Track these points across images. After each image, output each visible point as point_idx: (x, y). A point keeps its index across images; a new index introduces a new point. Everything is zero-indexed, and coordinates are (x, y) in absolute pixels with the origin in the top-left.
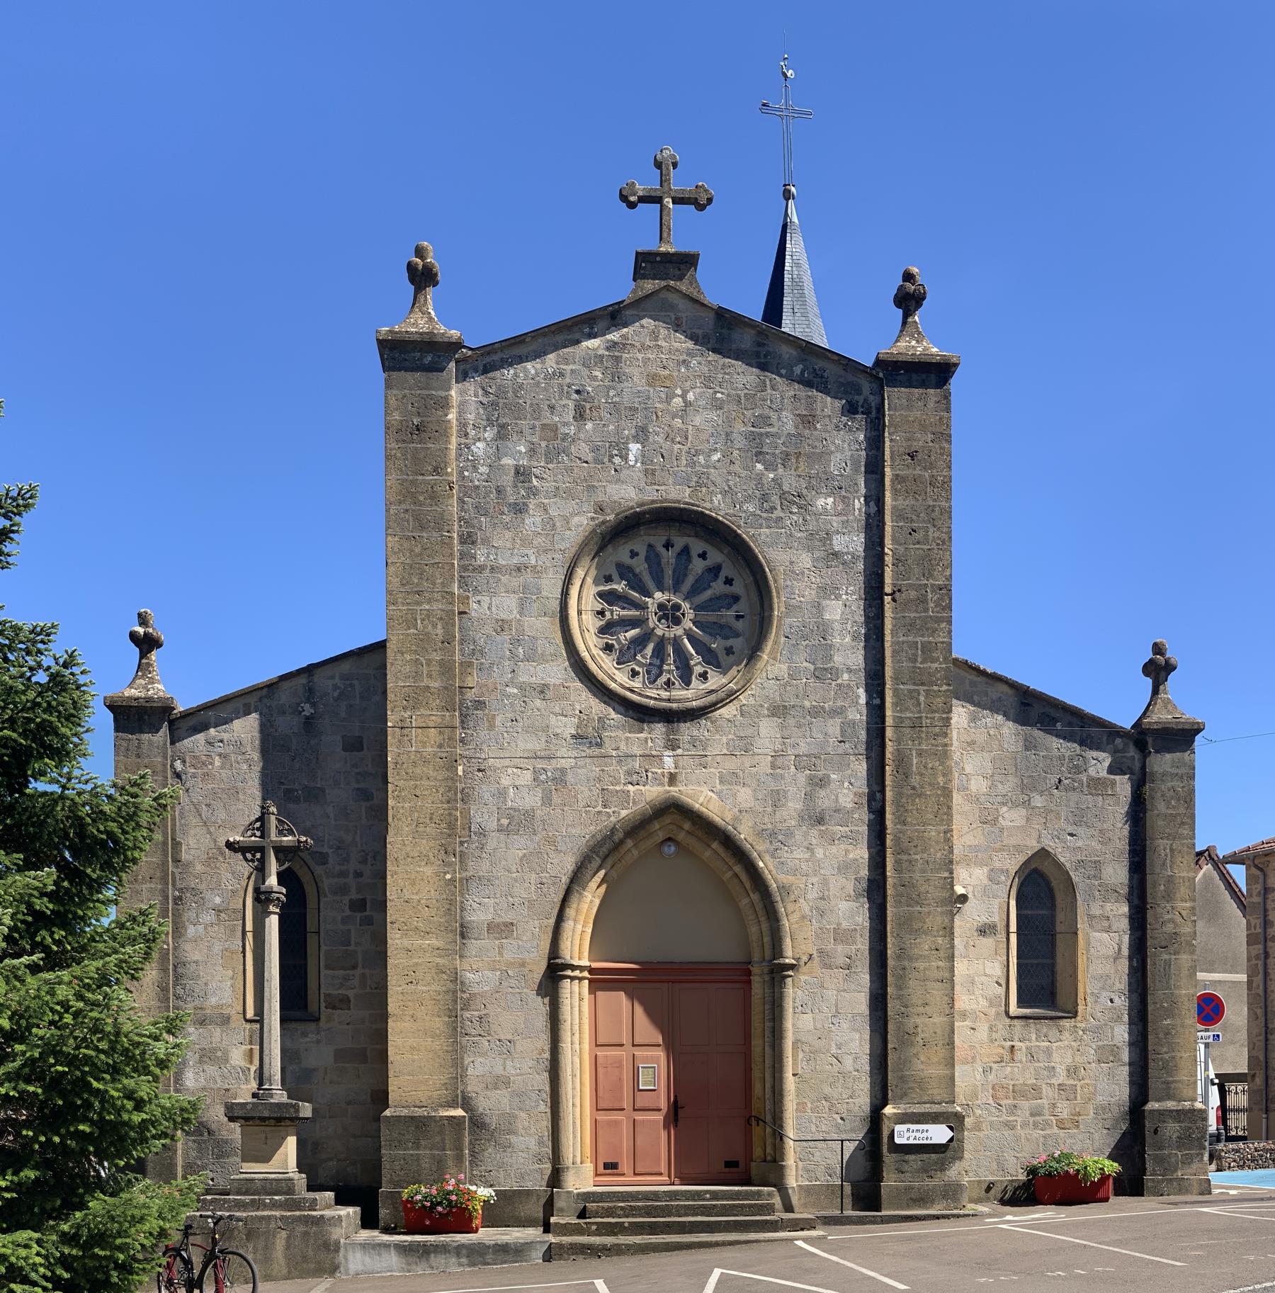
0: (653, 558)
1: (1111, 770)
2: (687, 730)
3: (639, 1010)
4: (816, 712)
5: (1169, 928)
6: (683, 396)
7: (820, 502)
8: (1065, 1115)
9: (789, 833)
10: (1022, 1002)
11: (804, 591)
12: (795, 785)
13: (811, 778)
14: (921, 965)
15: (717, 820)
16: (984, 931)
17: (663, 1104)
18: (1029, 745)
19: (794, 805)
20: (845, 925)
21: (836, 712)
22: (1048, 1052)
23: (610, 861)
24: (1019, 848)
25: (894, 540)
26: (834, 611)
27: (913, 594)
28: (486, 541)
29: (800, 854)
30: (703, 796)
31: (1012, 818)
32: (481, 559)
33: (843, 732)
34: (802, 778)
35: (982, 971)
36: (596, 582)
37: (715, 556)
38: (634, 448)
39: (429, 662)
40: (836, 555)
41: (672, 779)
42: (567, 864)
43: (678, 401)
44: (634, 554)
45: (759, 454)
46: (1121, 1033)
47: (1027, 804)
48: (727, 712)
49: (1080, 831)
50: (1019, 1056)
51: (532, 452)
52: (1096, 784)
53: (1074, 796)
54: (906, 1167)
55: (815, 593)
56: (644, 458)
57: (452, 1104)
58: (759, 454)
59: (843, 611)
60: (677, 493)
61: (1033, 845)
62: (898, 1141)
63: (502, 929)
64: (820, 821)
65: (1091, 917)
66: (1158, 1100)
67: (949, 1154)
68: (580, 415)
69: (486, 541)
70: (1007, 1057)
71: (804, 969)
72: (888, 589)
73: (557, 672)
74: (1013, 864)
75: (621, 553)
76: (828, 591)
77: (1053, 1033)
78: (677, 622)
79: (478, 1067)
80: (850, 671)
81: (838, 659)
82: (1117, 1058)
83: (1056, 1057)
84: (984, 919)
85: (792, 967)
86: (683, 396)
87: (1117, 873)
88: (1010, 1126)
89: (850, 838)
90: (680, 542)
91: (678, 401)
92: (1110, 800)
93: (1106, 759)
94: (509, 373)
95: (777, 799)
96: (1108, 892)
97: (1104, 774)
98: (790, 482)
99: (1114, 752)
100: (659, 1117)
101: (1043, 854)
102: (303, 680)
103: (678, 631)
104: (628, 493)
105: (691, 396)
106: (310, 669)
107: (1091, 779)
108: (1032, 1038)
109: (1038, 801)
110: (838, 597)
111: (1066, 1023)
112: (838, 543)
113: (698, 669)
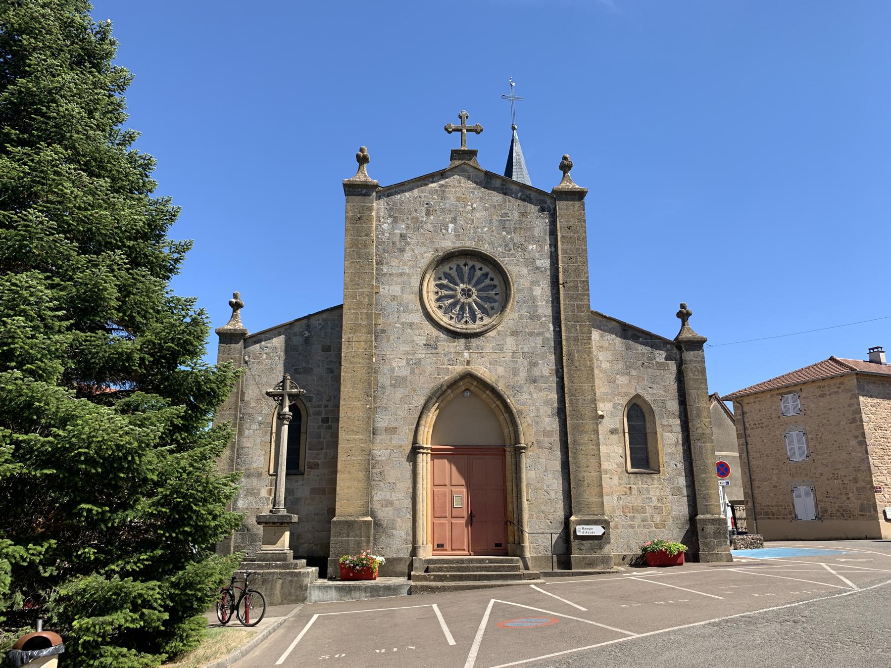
0: (459, 270)
1: (666, 359)
2: (474, 342)
3: (454, 468)
4: (531, 334)
5: (700, 431)
6: (472, 206)
7: (530, 247)
8: (658, 521)
9: (521, 387)
10: (633, 466)
11: (524, 283)
12: (523, 365)
13: (530, 362)
14: (584, 448)
15: (488, 381)
16: (613, 432)
17: (465, 514)
18: (628, 348)
19: (523, 374)
20: (548, 428)
21: (539, 334)
22: (648, 490)
23: (440, 399)
24: (626, 394)
25: (563, 262)
26: (537, 291)
27: (572, 284)
28: (387, 263)
29: (526, 396)
30: (482, 370)
31: (622, 380)
32: (385, 271)
33: (543, 342)
34: (526, 362)
35: (614, 451)
36: (435, 280)
37: (486, 269)
38: (451, 226)
39: (361, 313)
40: (537, 268)
41: (468, 363)
42: (420, 401)
43: (469, 208)
44: (451, 269)
45: (504, 228)
46: (682, 481)
47: (629, 374)
48: (492, 334)
49: (654, 386)
50: (634, 492)
51: (408, 227)
52: (660, 365)
53: (650, 370)
54: (583, 547)
55: (529, 283)
56: (455, 230)
57: (366, 515)
58: (504, 228)
59: (542, 291)
60: (469, 244)
61: (633, 393)
62: (578, 534)
63: (391, 430)
64: (535, 381)
65: (663, 426)
66: (703, 514)
67: (603, 540)
68: (428, 213)
69: (387, 263)
70: (628, 492)
71: (530, 449)
72: (561, 282)
73: (418, 317)
74: (624, 401)
75: (446, 268)
76: (534, 283)
77: (649, 481)
78: (470, 296)
79: (379, 496)
80: (545, 316)
81: (540, 311)
82: (681, 493)
83: (652, 493)
84: (612, 426)
85: (524, 448)
86: (472, 206)
87: (673, 405)
88: (632, 527)
89: (548, 389)
90: (470, 264)
91: (469, 208)
92: (667, 372)
93: (664, 354)
94: (398, 197)
95: (515, 372)
96: (670, 414)
97: (663, 360)
98: (517, 239)
99: (667, 351)
100: (463, 521)
101: (638, 396)
102: (305, 321)
103: (470, 300)
104: (448, 244)
105: (475, 205)
106: (309, 317)
107: (657, 363)
108: (639, 483)
109: (634, 372)
110: (539, 286)
111: (655, 476)
112: (539, 263)
113: (479, 316)
